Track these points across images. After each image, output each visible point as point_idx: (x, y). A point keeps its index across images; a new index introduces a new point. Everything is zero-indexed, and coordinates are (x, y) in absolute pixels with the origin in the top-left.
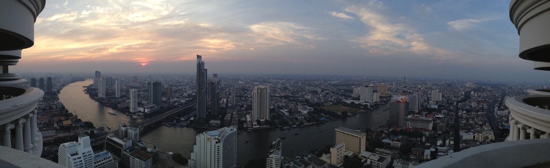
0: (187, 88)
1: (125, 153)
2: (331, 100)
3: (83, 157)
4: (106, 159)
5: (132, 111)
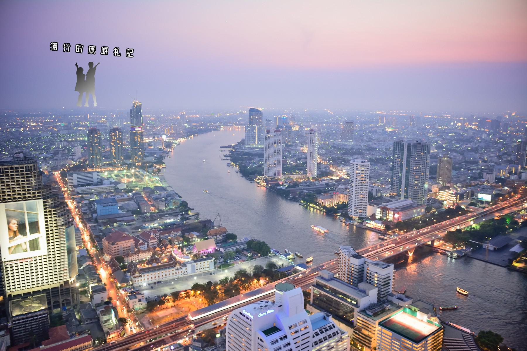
2: (421, 209)
4: (324, 330)
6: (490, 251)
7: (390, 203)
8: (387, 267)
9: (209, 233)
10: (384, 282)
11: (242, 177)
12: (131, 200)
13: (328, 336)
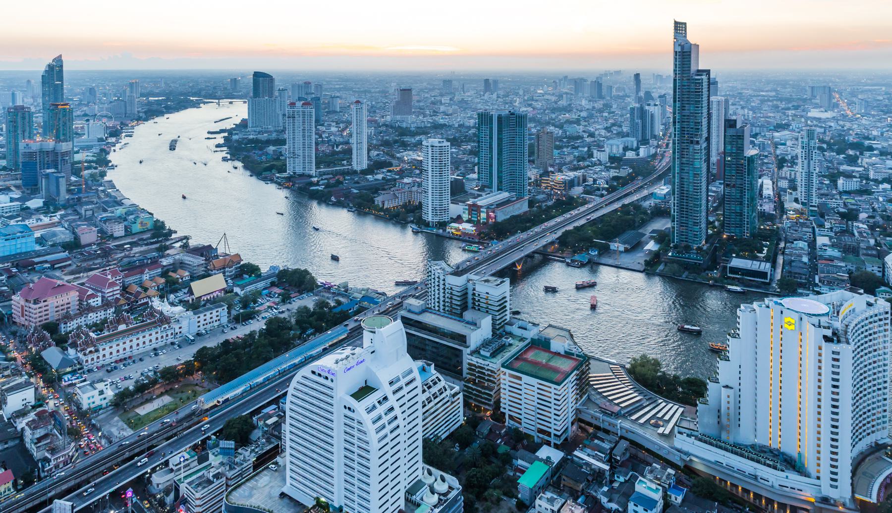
0: (599, 128)
1: (475, 360)
3: (395, 392)
5: (430, 219)
6: (621, 252)
7: (480, 198)
8: (501, 282)
9: (212, 266)
10: (500, 305)
11: (251, 176)
12: (56, 226)
13: (433, 395)
